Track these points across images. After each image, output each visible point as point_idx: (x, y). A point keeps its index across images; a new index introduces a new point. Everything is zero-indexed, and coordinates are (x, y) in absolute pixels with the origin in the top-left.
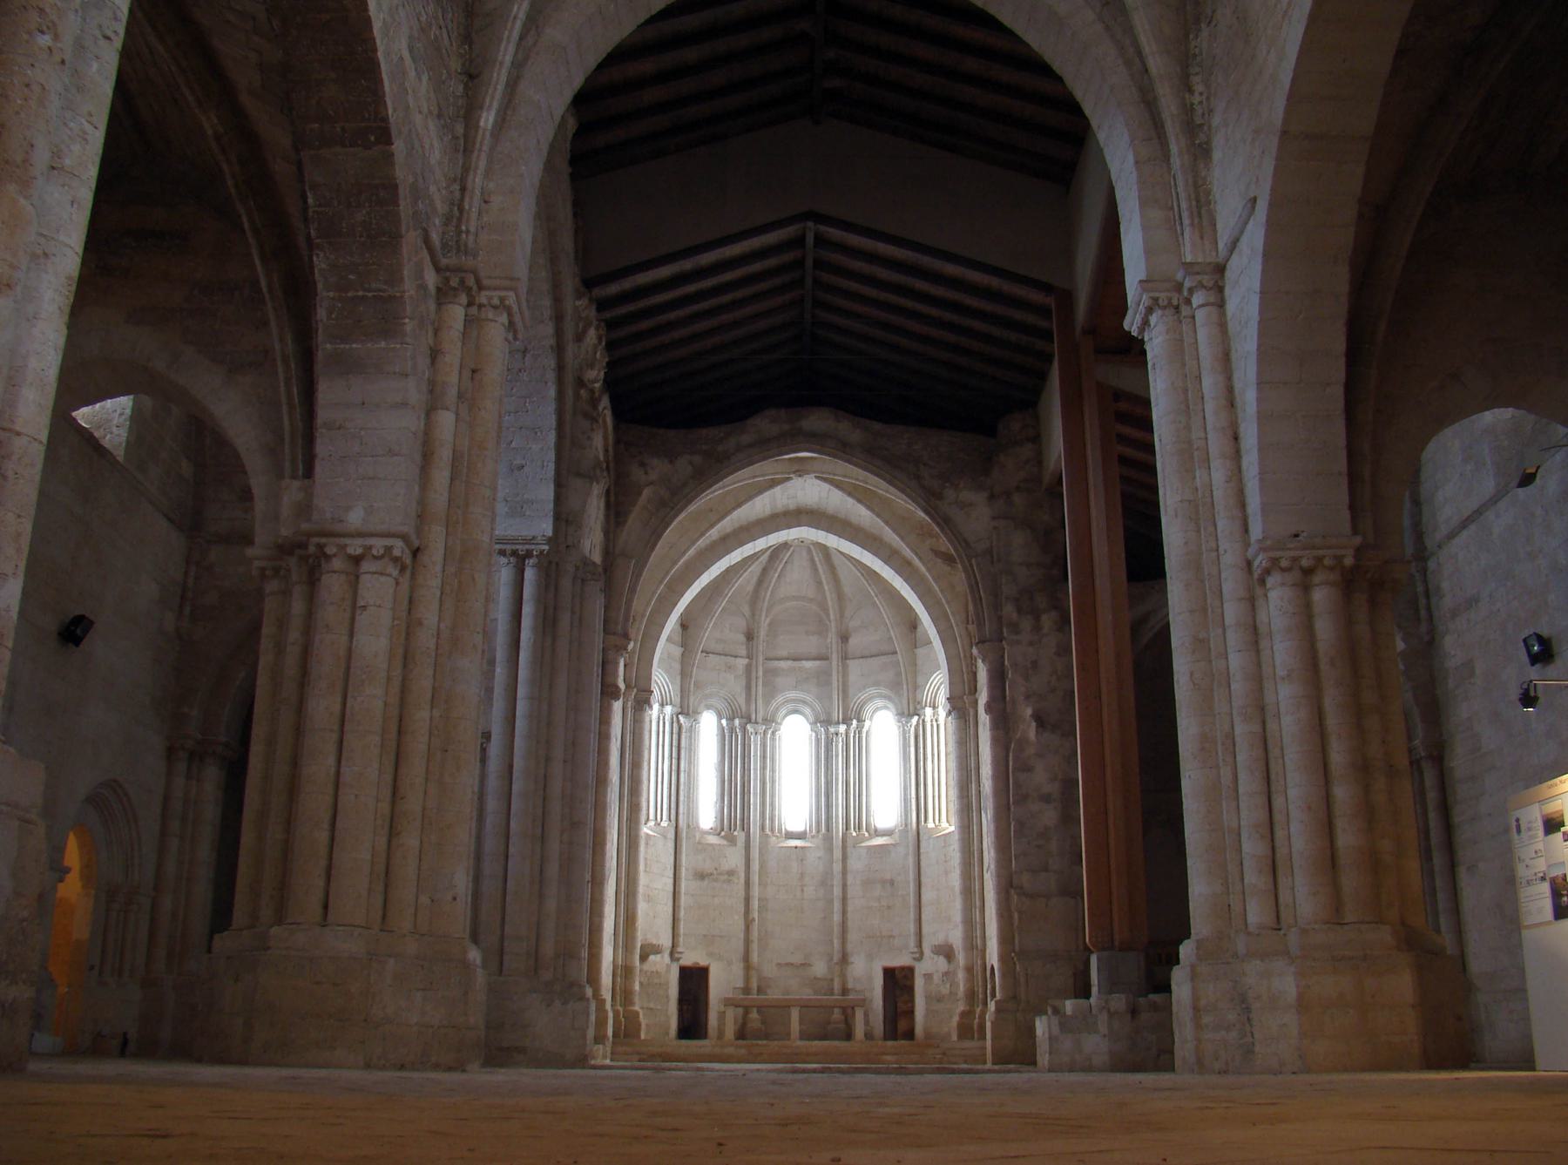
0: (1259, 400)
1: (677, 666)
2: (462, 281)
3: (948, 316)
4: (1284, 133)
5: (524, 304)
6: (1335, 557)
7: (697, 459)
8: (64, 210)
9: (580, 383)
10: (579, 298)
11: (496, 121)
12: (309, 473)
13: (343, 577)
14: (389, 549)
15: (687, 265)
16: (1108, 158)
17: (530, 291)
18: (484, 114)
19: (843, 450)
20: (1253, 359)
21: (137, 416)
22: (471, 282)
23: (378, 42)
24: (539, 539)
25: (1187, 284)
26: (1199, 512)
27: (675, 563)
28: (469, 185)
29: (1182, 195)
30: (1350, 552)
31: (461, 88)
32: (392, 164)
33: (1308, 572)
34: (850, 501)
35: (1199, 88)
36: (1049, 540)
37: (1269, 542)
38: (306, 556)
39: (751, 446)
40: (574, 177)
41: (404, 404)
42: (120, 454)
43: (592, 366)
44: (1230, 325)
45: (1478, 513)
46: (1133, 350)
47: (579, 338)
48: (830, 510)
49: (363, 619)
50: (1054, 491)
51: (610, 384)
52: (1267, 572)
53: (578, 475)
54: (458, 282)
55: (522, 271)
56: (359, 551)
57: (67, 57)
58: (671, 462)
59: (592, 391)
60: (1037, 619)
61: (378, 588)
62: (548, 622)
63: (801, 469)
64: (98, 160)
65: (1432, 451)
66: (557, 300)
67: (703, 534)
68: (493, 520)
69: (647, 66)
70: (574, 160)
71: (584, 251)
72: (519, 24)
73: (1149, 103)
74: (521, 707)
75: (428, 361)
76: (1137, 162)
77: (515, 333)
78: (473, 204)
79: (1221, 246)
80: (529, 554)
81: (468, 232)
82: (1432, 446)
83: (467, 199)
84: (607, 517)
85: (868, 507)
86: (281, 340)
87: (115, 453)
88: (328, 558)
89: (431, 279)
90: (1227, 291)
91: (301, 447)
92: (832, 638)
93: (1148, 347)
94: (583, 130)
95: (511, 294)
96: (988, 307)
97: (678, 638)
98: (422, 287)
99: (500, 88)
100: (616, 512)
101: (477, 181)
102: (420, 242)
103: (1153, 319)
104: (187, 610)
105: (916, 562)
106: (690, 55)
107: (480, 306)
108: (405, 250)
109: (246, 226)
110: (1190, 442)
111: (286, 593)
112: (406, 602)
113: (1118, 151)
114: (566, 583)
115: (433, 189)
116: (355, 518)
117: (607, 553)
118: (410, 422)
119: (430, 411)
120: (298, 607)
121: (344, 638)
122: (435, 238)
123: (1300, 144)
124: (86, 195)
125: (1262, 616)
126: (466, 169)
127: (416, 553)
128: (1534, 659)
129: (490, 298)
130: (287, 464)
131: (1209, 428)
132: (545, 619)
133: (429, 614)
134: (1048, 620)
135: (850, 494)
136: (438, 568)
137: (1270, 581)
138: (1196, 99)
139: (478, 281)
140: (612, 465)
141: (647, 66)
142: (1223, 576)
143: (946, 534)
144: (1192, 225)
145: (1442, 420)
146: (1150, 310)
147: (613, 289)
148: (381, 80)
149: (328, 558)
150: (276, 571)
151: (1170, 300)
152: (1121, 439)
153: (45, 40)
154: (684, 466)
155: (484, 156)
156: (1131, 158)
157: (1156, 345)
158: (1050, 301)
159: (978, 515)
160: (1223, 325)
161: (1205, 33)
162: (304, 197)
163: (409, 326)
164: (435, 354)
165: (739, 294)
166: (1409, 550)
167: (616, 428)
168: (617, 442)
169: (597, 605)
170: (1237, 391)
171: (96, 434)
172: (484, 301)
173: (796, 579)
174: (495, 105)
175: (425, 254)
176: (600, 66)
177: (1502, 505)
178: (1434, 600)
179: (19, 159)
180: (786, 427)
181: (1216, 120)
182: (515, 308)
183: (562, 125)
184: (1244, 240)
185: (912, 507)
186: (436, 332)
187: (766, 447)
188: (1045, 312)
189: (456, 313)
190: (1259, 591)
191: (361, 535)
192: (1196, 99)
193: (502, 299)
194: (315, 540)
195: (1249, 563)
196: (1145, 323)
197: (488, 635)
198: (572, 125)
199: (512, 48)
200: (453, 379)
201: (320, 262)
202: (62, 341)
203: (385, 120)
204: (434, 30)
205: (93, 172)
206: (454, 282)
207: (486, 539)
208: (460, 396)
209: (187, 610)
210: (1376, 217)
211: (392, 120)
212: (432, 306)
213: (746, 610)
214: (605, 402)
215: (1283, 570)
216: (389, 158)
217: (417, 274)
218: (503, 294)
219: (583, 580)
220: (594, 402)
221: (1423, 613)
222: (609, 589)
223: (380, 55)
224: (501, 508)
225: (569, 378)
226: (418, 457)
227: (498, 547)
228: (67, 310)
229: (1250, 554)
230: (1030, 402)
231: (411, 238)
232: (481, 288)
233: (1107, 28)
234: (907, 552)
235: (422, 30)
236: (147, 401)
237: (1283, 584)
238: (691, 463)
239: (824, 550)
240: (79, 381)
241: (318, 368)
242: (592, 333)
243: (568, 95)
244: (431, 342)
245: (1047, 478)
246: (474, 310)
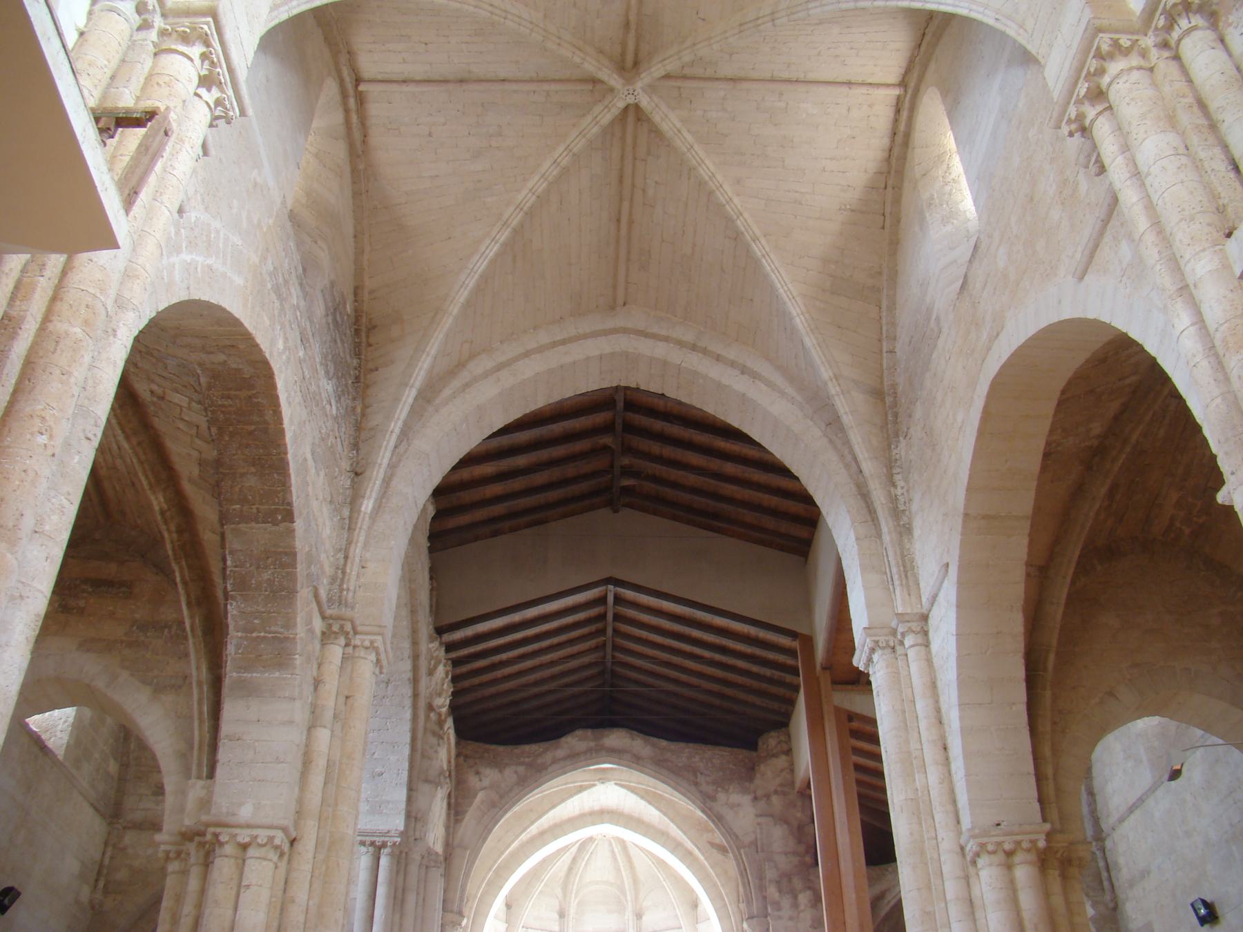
0: (961, 718)
2: (342, 627)
3: (718, 657)
4: (966, 515)
5: (389, 646)
6: (1031, 841)
7: (521, 769)
8: (41, 561)
9: (430, 708)
10: (432, 642)
11: (374, 508)
12: (211, 775)
13: (232, 861)
14: (271, 839)
15: (516, 617)
16: (835, 536)
17: (394, 636)
18: (365, 502)
19: (636, 761)
20: (954, 686)
21: (78, 725)
22: (348, 627)
23: (289, 447)
24: (393, 833)
25: (900, 630)
26: (921, 809)
27: (502, 853)
28: (351, 555)
29: (893, 563)
30: (1043, 836)
31: (349, 482)
32: (294, 537)
33: (1010, 854)
34: (643, 803)
35: (900, 483)
36: (802, 834)
37: (977, 831)
38: (203, 843)
40: (431, 550)
41: (291, 722)
42: (60, 753)
43: (440, 695)
44: (935, 660)
45: (1141, 800)
46: (860, 681)
47: (431, 673)
48: (626, 811)
49: (245, 897)
50: (804, 794)
51: (454, 708)
52: (978, 855)
53: (427, 781)
54: (338, 628)
55: (388, 619)
56: (247, 840)
57: (57, 451)
59: (440, 715)
60: (795, 897)
61: (261, 872)
62: (398, 900)
63: (603, 777)
64: (70, 528)
65: (1099, 753)
66: (415, 644)
67: (524, 830)
68: (357, 817)
69: (488, 469)
70: (432, 537)
71: (436, 608)
72: (394, 437)
73: (864, 495)
75: (312, 688)
76: (857, 539)
77: (381, 668)
78: (353, 569)
79: (924, 600)
80: (384, 845)
81: (348, 590)
82: (1099, 748)
83: (349, 565)
84: (448, 815)
85: (657, 808)
86: (198, 668)
87: (57, 752)
88: (221, 844)
89: (318, 625)
90: (931, 634)
91: (207, 754)
92: (629, 915)
93: (872, 679)
94: (439, 515)
95: (379, 638)
96: (748, 649)
97: (503, 915)
98: (311, 631)
99: (378, 483)
100: (456, 810)
101: (357, 551)
102: (311, 596)
103: (875, 657)
104: (101, 884)
105: (696, 852)
106: (521, 461)
107: (355, 647)
108: (299, 603)
109: (178, 579)
110: (909, 753)
111: (185, 873)
112: (282, 883)
113: (842, 530)
114: (413, 869)
115: (323, 556)
116: (246, 812)
117: (448, 845)
118: (295, 736)
119: (311, 728)
120: (193, 884)
121: (230, 912)
122: (323, 594)
123: (980, 522)
124: (58, 552)
125: (976, 892)
126: (349, 543)
127: (293, 842)
128: (1203, 921)
129: (363, 641)
130: (194, 768)
131: (924, 739)
132: (395, 897)
133: (301, 893)
134: (804, 898)
135: (642, 798)
136: (310, 855)
137: (981, 862)
138: (899, 491)
139: (354, 628)
140: (453, 773)
141: (488, 469)
142: (942, 859)
143: (719, 829)
144: (901, 585)
145: (1104, 729)
146: (873, 650)
147: (458, 635)
148: (289, 476)
149: (221, 844)
150: (179, 854)
151: (887, 642)
152: (856, 751)
153: (42, 439)
154: (510, 774)
155: (363, 533)
156: (852, 537)
157: (879, 677)
158: (795, 644)
159: (744, 812)
160: (929, 661)
161: (903, 442)
162: (224, 560)
163: (298, 660)
164: (317, 683)
165: (555, 640)
166: (1089, 833)
167: (457, 744)
168: (458, 755)
169: (437, 886)
170: (943, 711)
171: (43, 737)
172: (358, 642)
173: (599, 869)
174: (374, 495)
175: (314, 605)
176: (454, 468)
177: (1159, 793)
178: (1113, 874)
179: (11, 524)
180: (592, 744)
181: (915, 507)
182: (382, 649)
183: (424, 509)
184: (941, 595)
185: (692, 807)
186: (320, 665)
187: (575, 760)
188: (791, 653)
189: (336, 652)
190: (971, 870)
191: (249, 826)
192: (899, 491)
193: (372, 642)
194: (212, 830)
195: (962, 848)
196: (870, 660)
197: (348, 912)
198: (431, 511)
199: (388, 454)
200: (330, 703)
201: (232, 609)
202: (25, 665)
203: (290, 504)
204: (331, 440)
205: (65, 536)
206: (335, 628)
207: (350, 832)
208: (335, 716)
209: (101, 884)
210: (1040, 573)
211: (295, 504)
212: (318, 646)
213: (559, 891)
214: (449, 724)
215: (990, 853)
216: (291, 532)
217: (306, 620)
218: (373, 637)
220: (441, 723)
221: (1106, 884)
222: (447, 875)
223: (290, 457)
224: (364, 807)
225: (422, 704)
226: (299, 766)
227: (360, 838)
228: (33, 640)
229: (962, 841)
230: (782, 722)
231: (304, 593)
232: (356, 633)
233: (831, 441)
234: (689, 845)
235: (323, 439)
236: (88, 712)
237: (990, 865)
238: (516, 772)
239: (623, 843)
240: (36, 694)
241: (225, 691)
242: (441, 668)
243: (430, 492)
244: (315, 674)
245: (798, 784)
246: (350, 650)
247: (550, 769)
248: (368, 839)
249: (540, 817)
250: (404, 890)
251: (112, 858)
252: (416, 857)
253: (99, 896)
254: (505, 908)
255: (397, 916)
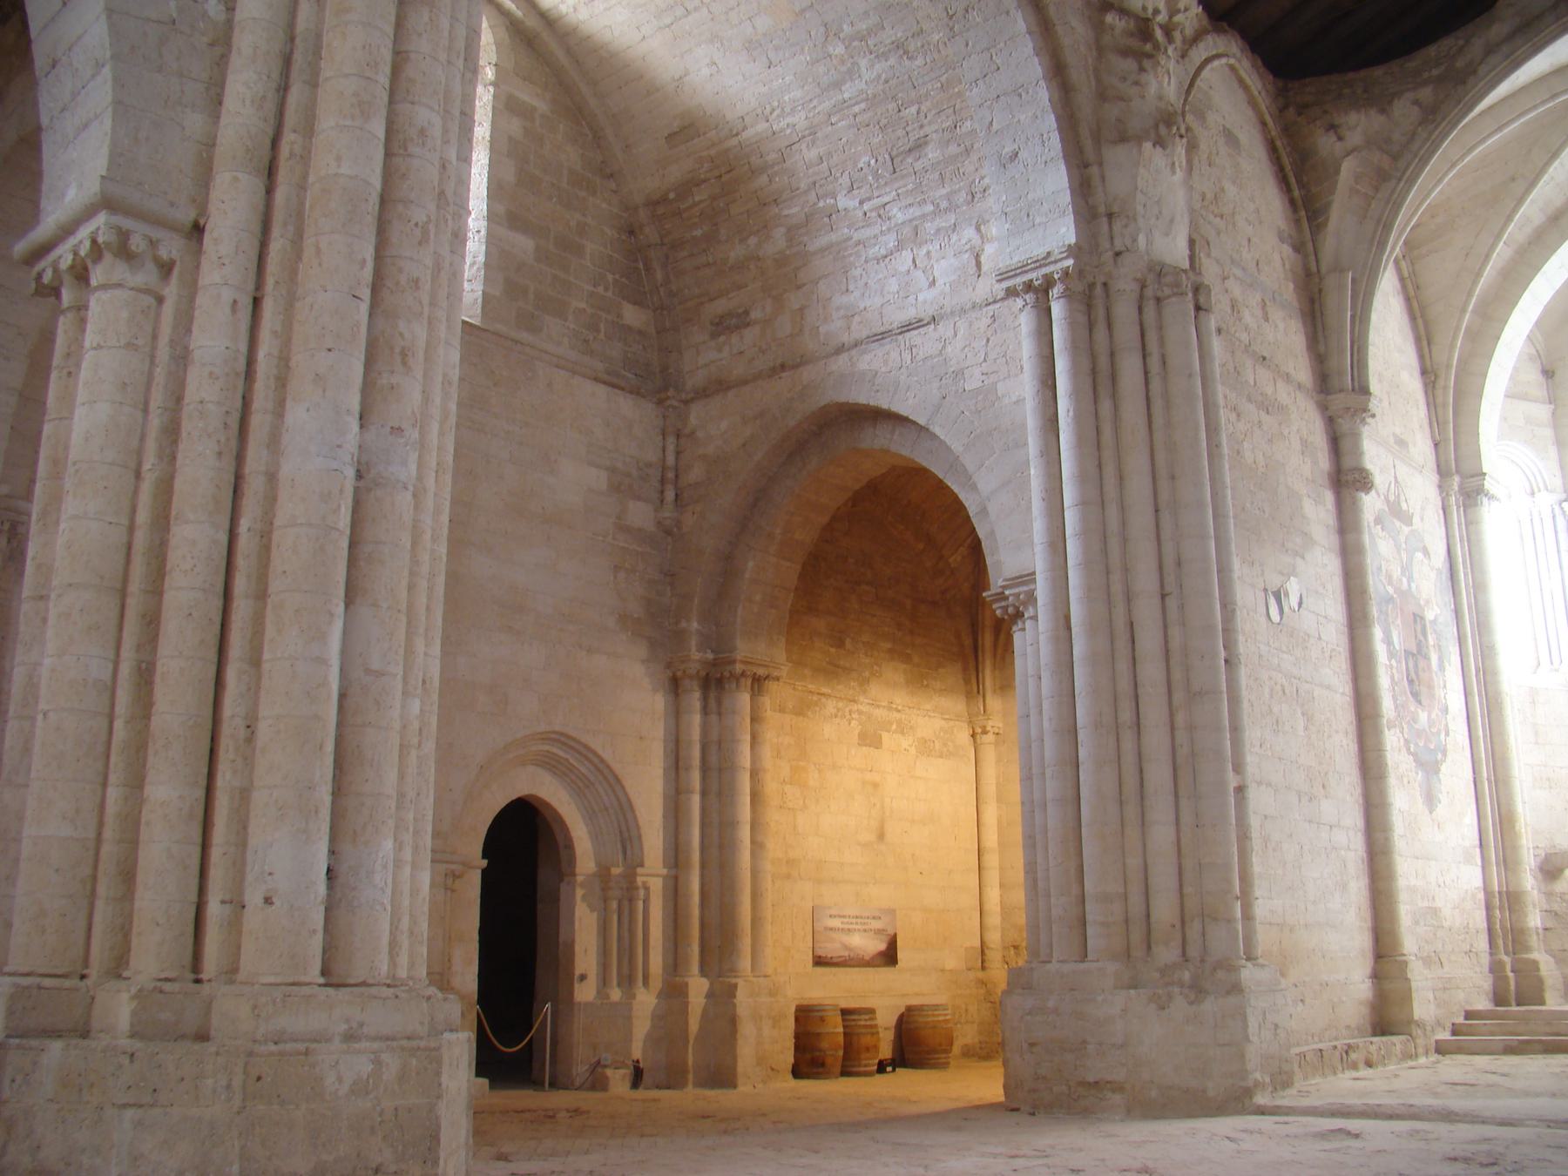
1: (1548, 433)
7: (1426, 93)
24: (1056, 255)
27: (1479, 274)
39: (1511, 37)
58: (1383, 111)
74: (1071, 518)
80: (1049, 283)
114: (1124, 311)
154: (1404, 110)
209: (670, 495)
219: (1158, 300)
238: (1416, 102)
247: (1482, 70)
248: (1019, 280)
249: (1532, 185)
250: (1112, 354)
251: (678, 453)
252: (1125, 285)
253: (668, 513)
254: (1541, 379)
255: (1106, 407)
